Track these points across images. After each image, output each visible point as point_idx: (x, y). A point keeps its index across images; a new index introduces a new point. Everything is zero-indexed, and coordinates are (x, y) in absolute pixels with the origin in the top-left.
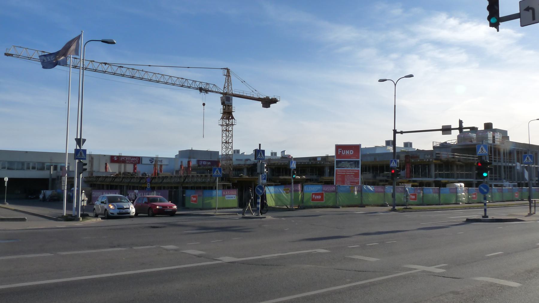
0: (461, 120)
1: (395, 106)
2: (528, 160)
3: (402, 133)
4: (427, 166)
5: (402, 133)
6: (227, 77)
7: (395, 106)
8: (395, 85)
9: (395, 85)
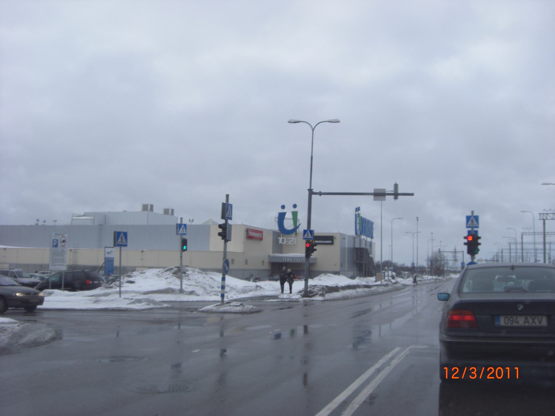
0: (397, 183)
1: (312, 157)
2: (473, 224)
3: (320, 194)
4: (331, 242)
5: (320, 194)
6: (9, 308)
7: (312, 157)
8: (313, 130)
9: (313, 130)
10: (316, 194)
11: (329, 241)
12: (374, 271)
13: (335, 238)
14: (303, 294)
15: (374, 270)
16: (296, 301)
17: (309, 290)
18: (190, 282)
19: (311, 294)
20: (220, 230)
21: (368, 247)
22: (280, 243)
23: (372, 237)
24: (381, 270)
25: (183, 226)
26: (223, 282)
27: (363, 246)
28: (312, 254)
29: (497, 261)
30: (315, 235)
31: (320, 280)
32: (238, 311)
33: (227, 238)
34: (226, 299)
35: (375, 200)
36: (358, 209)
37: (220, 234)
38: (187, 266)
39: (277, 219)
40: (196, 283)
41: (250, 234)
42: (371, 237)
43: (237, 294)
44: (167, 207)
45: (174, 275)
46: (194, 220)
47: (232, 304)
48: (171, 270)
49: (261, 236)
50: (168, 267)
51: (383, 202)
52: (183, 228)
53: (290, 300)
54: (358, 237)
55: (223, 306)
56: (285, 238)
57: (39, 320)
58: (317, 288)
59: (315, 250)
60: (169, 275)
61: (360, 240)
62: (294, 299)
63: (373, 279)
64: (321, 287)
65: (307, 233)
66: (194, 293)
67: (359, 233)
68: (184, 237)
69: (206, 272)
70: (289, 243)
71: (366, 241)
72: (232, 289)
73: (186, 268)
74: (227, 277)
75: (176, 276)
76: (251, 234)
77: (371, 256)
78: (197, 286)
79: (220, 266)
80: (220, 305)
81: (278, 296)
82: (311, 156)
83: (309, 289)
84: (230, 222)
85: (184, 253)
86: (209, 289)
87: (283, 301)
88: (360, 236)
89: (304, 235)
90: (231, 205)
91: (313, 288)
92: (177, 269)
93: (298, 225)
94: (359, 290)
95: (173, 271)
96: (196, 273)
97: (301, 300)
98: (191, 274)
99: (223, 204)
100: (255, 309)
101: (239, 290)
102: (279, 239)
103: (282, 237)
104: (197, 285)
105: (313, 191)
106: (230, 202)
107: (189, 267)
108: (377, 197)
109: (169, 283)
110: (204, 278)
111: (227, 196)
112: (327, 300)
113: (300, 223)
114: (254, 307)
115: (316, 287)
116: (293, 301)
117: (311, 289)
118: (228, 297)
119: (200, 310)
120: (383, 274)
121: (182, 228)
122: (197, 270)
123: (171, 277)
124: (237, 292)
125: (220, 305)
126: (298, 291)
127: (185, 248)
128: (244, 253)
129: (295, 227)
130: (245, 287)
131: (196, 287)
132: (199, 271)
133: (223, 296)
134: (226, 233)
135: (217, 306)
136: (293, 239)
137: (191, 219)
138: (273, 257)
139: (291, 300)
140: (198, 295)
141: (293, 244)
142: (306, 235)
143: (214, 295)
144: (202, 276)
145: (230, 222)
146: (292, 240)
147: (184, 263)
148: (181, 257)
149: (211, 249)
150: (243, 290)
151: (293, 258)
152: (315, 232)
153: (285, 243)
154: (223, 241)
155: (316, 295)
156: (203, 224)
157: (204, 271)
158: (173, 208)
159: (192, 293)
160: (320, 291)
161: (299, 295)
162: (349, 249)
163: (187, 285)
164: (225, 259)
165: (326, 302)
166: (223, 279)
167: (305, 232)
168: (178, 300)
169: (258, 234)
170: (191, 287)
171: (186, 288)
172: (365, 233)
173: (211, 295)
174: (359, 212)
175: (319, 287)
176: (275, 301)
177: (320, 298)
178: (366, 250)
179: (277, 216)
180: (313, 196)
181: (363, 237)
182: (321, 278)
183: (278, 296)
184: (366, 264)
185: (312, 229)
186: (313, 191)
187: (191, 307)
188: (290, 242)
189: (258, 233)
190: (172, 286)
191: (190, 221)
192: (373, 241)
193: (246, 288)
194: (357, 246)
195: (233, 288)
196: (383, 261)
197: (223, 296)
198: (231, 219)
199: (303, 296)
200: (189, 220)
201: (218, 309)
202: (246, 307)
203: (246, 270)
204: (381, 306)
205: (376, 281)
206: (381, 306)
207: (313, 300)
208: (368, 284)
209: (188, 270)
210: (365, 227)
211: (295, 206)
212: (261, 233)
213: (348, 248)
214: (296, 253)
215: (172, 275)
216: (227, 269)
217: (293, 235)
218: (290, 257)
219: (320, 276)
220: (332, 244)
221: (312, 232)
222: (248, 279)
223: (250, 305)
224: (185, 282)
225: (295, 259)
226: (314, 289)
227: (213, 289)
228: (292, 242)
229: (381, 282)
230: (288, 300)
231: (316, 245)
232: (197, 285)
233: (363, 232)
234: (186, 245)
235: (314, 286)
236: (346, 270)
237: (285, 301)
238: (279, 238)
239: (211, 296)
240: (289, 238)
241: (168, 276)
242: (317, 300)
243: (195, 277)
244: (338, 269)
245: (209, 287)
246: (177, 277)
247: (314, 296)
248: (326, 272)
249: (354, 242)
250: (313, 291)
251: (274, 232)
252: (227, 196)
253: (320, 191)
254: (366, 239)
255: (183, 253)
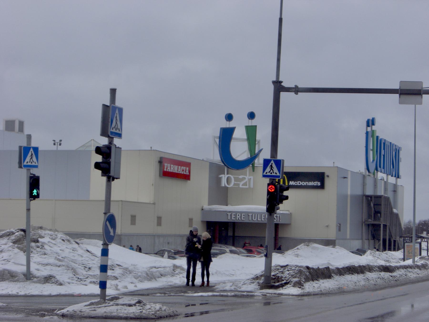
1: (281, 20)
3: (297, 90)
5: (297, 90)
7: (281, 20)
10: (288, 90)
11: (316, 182)
12: (402, 239)
13: (328, 176)
14: (261, 281)
15: (401, 237)
16: (247, 296)
17: (274, 275)
18: (45, 258)
19: (278, 282)
20: (99, 158)
21: (390, 195)
22: (223, 185)
23: (398, 176)
24: (414, 238)
25: (32, 150)
26: (105, 258)
27: (381, 192)
28: (280, 206)
29: (329, 289)
30: (286, 170)
31: (297, 256)
32: (132, 315)
33: (112, 174)
34: (110, 291)
35: (401, 103)
36: (371, 123)
37: (97, 166)
38: (41, 228)
39: (217, 140)
40: (59, 260)
41: (166, 167)
42: (395, 176)
43: (135, 280)
44: (10, 117)
45: (16, 245)
46: (62, 142)
47: (120, 301)
48: (9, 235)
49: (187, 171)
50: (3, 230)
51: (417, 106)
52: (32, 154)
53: (237, 293)
54: (372, 175)
55: (104, 305)
56: (232, 177)
57: (159, 274)
58: (288, 271)
59: (287, 198)
60: (6, 244)
61: (375, 181)
62: (244, 292)
63: (399, 254)
64: (297, 268)
65: (270, 164)
66: (53, 280)
67: (372, 167)
68: (35, 172)
69: (78, 241)
70: (241, 186)
71: (386, 183)
72: (127, 271)
73: (40, 232)
74: (113, 248)
75: (18, 248)
76: (169, 168)
77: (395, 211)
78: (59, 266)
79: (99, 229)
80: (97, 303)
81: (214, 286)
82: (279, 17)
83: (273, 273)
84: (117, 141)
85: (34, 203)
86: (82, 272)
87: (222, 296)
88: (374, 174)
89: (264, 170)
90: (121, 110)
91: (282, 270)
92: (22, 233)
93: (257, 151)
94: (371, 275)
95: (13, 237)
96: (59, 240)
97: (259, 293)
98: (49, 242)
99: (105, 107)
100: (165, 310)
101: (139, 274)
102: (221, 178)
103: (228, 174)
104: (60, 263)
105: (282, 84)
106: (118, 103)
107: (45, 229)
108: (404, 97)
109: (4, 260)
110: (74, 250)
111: (113, 92)
112: (308, 295)
113: (261, 149)
114: (164, 308)
115: (287, 269)
116: (243, 296)
117: (277, 272)
118: (119, 287)
119: (58, 312)
120: (417, 246)
121: (30, 154)
122: (60, 235)
123: (10, 249)
124: (136, 278)
125: (97, 303)
126: (253, 276)
127: (35, 192)
128: (154, 204)
129: (251, 155)
130: (152, 268)
131: (57, 268)
132: (65, 237)
133: (103, 285)
134: (109, 164)
135: (92, 304)
136: (247, 177)
137: (57, 141)
138: (210, 212)
139: (240, 293)
140: (61, 284)
141: (247, 187)
142: (268, 169)
143: (91, 282)
144: (70, 246)
145: (117, 141)
146: (247, 180)
147: (34, 223)
148: (28, 210)
149: (92, 198)
150: (147, 274)
151: (247, 214)
152: (285, 165)
153: (231, 185)
154: (105, 179)
155: (286, 283)
156: (79, 149)
157: (73, 238)
158: (22, 119)
159: (48, 279)
160: (295, 277)
161: (255, 283)
162: (353, 197)
163: (39, 264)
164: (108, 214)
165: (306, 298)
166: (105, 252)
167: (266, 162)
168: (22, 293)
169: (182, 167)
170: (48, 267)
171: (38, 270)
172: (384, 168)
173: (85, 283)
174: (374, 128)
175: (293, 268)
176: (208, 296)
177: (295, 291)
178: (387, 199)
179: (218, 134)
180: (283, 95)
181: (380, 175)
182: (299, 252)
183: (214, 286)
184: (385, 226)
185: (279, 157)
186: (282, 84)
187: (44, 306)
188: (241, 183)
189: (181, 166)
190: (11, 267)
191: (54, 144)
192: (400, 182)
193: (154, 270)
194: (369, 192)
195: (129, 271)
196: (417, 221)
197: (103, 285)
198: (119, 135)
199: (263, 287)
200: (53, 142)
201: (95, 310)
202: (148, 307)
203: (159, 236)
204: (412, 306)
205: (404, 260)
206: (412, 306)
207: (281, 294)
208: (388, 264)
209: (43, 235)
210: (384, 156)
211: (251, 116)
212: (186, 167)
213: (353, 197)
214: (252, 205)
215: (12, 244)
216: (112, 234)
217: (248, 170)
218: (241, 213)
219: (298, 249)
220: (322, 187)
221: (279, 163)
222: (160, 253)
223: (155, 303)
224: (36, 258)
225: (252, 216)
226: (282, 273)
227: (90, 273)
228: (245, 184)
229: (414, 261)
230: (233, 294)
231: (287, 189)
232: (60, 263)
233: (380, 167)
234: (38, 188)
235: (282, 267)
236: (348, 237)
237: (227, 296)
238: (221, 176)
239: (86, 285)
240: (241, 177)
241: (3, 246)
242: (289, 295)
243: (56, 249)
244: (332, 234)
245: (83, 268)
246: (21, 249)
247: (282, 286)
248: (308, 241)
249: (364, 185)
250: (282, 277)
251: (212, 165)
252: (113, 92)
253: (295, 85)
254: (385, 180)
255: (32, 202)
